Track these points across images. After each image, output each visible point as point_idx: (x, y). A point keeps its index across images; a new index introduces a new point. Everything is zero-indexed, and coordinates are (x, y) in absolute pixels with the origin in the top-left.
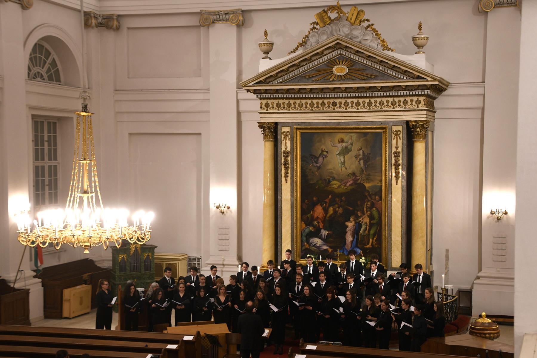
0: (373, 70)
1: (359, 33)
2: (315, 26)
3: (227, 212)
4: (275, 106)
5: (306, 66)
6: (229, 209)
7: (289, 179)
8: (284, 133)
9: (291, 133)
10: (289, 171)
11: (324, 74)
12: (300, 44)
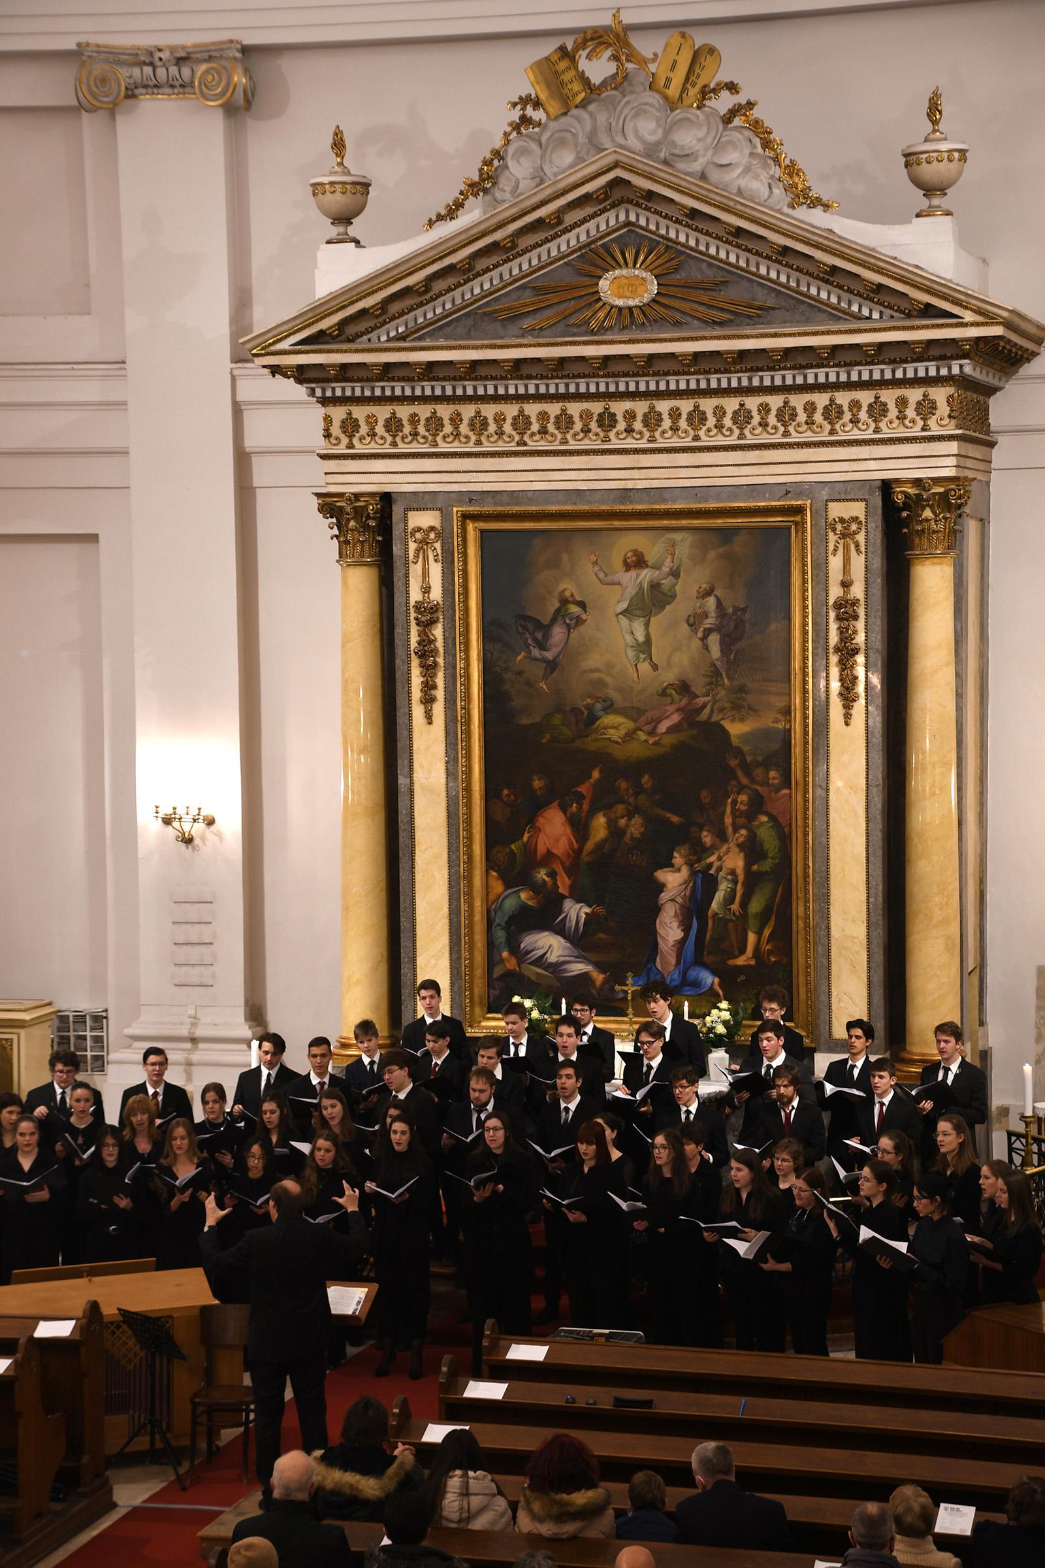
0: (755, 285)
1: (699, 140)
2: (529, 111)
3: (203, 838)
4: (380, 429)
5: (495, 274)
6: (213, 828)
7: (439, 709)
8: (418, 536)
9: (443, 534)
10: (440, 680)
11: (568, 303)
12: (472, 185)
